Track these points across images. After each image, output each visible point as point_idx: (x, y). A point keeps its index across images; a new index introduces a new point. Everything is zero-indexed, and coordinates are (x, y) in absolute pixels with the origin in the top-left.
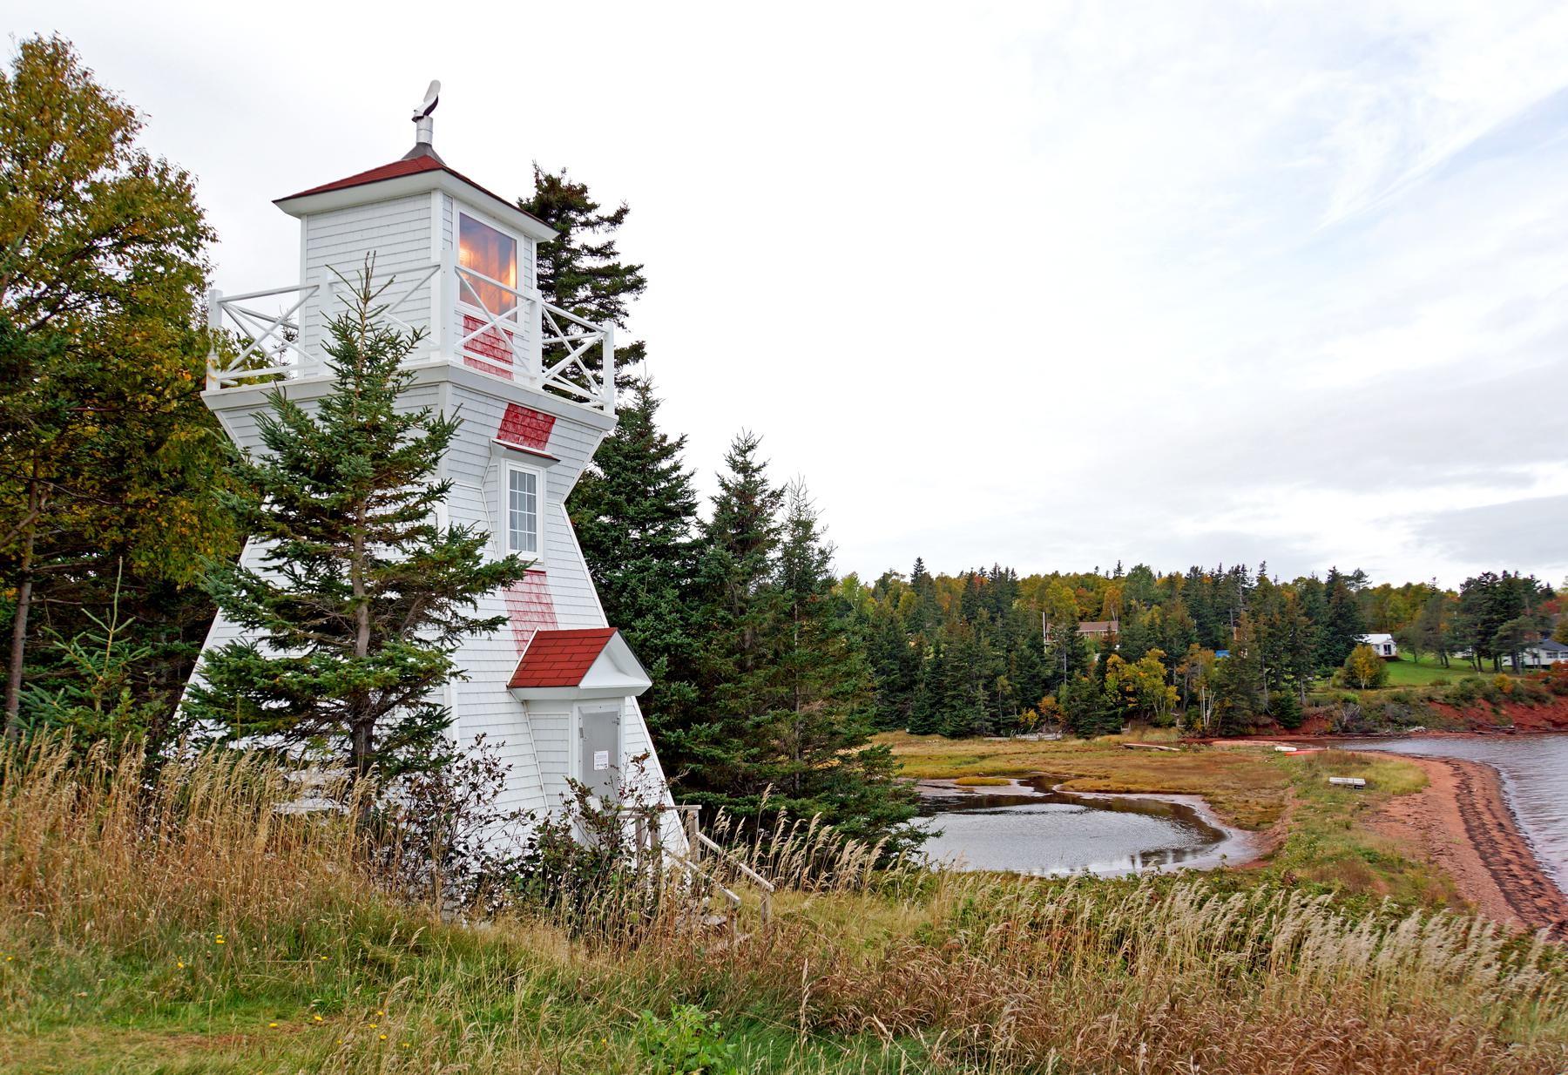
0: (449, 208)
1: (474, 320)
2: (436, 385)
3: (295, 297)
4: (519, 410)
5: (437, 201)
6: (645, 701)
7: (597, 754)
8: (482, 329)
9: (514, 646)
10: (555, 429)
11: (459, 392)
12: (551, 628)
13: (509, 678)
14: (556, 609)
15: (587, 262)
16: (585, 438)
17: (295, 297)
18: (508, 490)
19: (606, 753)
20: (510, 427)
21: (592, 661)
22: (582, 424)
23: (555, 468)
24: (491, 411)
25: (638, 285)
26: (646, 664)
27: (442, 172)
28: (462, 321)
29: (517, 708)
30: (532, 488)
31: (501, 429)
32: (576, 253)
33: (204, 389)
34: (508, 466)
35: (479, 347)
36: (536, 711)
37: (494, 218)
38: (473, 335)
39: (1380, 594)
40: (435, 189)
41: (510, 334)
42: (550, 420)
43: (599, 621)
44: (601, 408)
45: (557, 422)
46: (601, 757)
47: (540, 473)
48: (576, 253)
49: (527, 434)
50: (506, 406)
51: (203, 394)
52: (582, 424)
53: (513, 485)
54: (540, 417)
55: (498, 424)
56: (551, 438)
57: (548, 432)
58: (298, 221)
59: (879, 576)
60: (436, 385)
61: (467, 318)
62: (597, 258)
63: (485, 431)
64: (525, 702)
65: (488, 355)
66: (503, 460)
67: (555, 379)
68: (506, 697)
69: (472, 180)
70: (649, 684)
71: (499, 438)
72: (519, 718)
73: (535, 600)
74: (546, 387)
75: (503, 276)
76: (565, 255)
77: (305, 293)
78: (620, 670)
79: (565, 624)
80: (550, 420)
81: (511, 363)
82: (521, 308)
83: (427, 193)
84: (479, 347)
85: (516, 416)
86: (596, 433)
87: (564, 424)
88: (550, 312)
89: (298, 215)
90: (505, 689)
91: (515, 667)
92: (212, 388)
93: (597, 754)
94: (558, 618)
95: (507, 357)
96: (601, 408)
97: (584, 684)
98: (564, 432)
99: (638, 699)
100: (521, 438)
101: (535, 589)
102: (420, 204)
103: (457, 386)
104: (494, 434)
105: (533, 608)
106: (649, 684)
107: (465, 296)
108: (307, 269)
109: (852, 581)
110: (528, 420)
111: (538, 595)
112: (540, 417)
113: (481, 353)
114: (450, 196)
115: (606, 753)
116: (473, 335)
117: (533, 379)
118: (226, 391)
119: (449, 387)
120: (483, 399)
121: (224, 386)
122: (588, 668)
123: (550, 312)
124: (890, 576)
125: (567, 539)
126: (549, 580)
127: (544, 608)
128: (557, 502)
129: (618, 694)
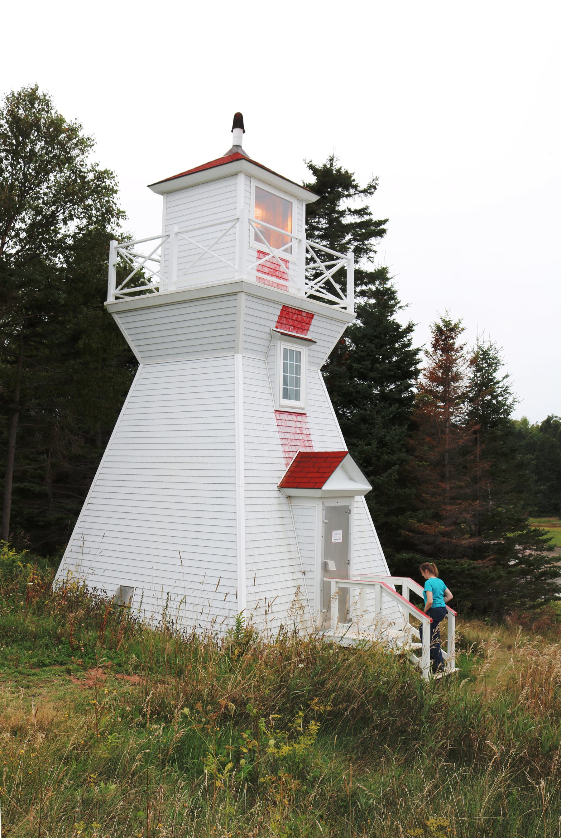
0: (248, 183)
1: (263, 253)
2: (236, 294)
3: (159, 241)
4: (290, 310)
5: (241, 180)
6: (368, 497)
7: (334, 532)
8: (267, 258)
9: (284, 461)
10: (313, 322)
11: (250, 298)
12: (308, 450)
13: (279, 481)
14: (312, 438)
15: (348, 220)
16: (334, 328)
17: (159, 241)
18: (282, 361)
19: (340, 532)
20: (284, 321)
21: (332, 472)
22: (332, 319)
23: (313, 347)
24: (271, 310)
25: (382, 233)
26: (368, 475)
27: (243, 161)
28: (256, 254)
29: (284, 501)
30: (298, 360)
31: (278, 322)
32: (342, 213)
33: (106, 300)
34: (282, 346)
35: (266, 270)
36: (295, 503)
37: (286, 192)
38: (261, 262)
39: (123, 277)
40: (241, 172)
41: (286, 261)
42: (311, 316)
43: (344, 447)
44: (345, 308)
45: (315, 317)
46: (337, 534)
47: (304, 351)
48: (342, 213)
49: (295, 325)
50: (281, 307)
51: (105, 303)
52: (332, 319)
53: (285, 358)
54: (304, 314)
55: (276, 318)
56: (311, 328)
57: (309, 324)
58: (161, 197)
59: (545, 418)
60: (236, 294)
61: (259, 252)
62: (356, 217)
63: (267, 323)
64: (289, 497)
65: (272, 275)
66: (279, 342)
67: (318, 291)
68: (276, 494)
69: (266, 166)
70: (371, 488)
71: (277, 327)
72: (285, 507)
73: (298, 432)
74: (311, 297)
75: (284, 227)
76: (335, 215)
77: (164, 239)
78: (351, 479)
79: (318, 448)
80: (311, 316)
81: (287, 280)
82: (294, 244)
83: (235, 175)
84: (266, 270)
85: (288, 314)
86: (342, 325)
87: (319, 318)
88: (311, 247)
89: (162, 193)
90: (277, 489)
91: (283, 474)
92: (111, 299)
93: (334, 532)
94: (314, 444)
95: (285, 276)
96: (345, 308)
97: (326, 487)
98: (320, 324)
99: (365, 497)
100: (292, 328)
101: (298, 425)
102: (231, 182)
103: (248, 294)
104: (273, 325)
105: (297, 437)
106: (371, 488)
107: (257, 239)
108: (166, 225)
109: (525, 422)
110: (295, 316)
111: (301, 428)
112: (304, 314)
113: (268, 274)
114: (250, 176)
115: (340, 532)
116: (261, 262)
117: (299, 290)
118: (118, 301)
119: (243, 296)
120: (266, 303)
121: (117, 298)
122: (328, 477)
123: (311, 247)
124: (552, 418)
125: (322, 393)
126: (308, 419)
127: (304, 437)
128: (316, 369)
129: (350, 495)
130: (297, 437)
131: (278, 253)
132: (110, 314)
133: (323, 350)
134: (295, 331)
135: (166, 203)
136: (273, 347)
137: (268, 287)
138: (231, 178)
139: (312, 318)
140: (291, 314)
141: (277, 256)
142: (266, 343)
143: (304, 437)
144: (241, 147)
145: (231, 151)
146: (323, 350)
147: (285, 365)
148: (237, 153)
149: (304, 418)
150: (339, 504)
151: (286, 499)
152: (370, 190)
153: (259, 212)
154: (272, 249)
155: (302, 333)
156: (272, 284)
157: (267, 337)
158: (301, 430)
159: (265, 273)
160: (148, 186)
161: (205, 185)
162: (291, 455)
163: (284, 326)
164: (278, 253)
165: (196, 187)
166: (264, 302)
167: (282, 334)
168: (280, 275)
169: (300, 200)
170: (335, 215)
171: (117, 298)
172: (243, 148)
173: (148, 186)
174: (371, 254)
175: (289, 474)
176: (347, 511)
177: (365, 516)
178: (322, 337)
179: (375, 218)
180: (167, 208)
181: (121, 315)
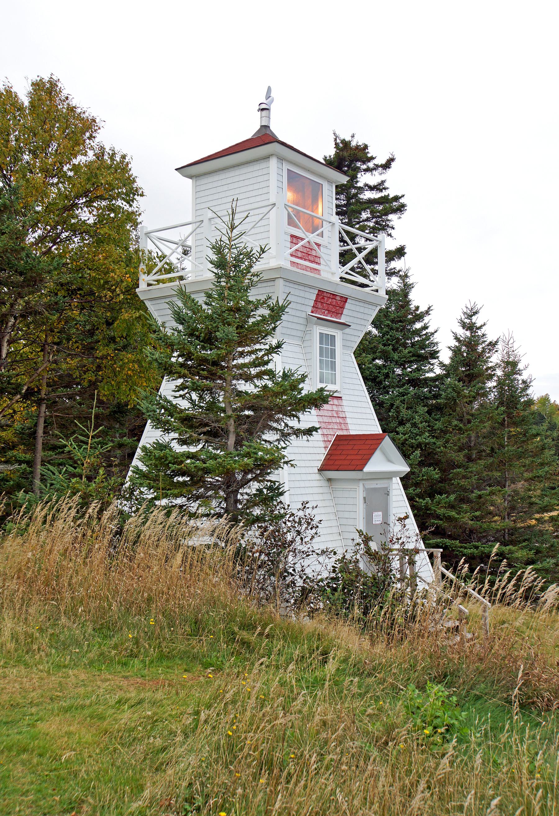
0: (280, 166)
2: (273, 280)
4: (325, 294)
5: (273, 163)
7: (375, 514)
8: (302, 243)
10: (347, 306)
11: (287, 284)
12: (345, 433)
13: (319, 464)
14: (348, 421)
15: (368, 195)
16: (366, 311)
18: (318, 345)
19: (380, 513)
20: (319, 305)
21: (372, 454)
23: (347, 330)
24: (307, 295)
25: (401, 209)
26: (406, 456)
28: (289, 239)
29: (325, 484)
30: (333, 343)
32: (361, 190)
34: (318, 330)
35: (300, 254)
38: (296, 247)
41: (318, 245)
42: (344, 300)
43: (375, 428)
44: (377, 291)
45: (348, 301)
46: (377, 516)
47: (338, 334)
48: (361, 190)
49: (330, 309)
50: (316, 292)
51: (137, 290)
52: (365, 302)
53: (321, 343)
54: (338, 298)
55: (312, 303)
56: (345, 312)
57: (343, 308)
60: (273, 280)
61: (292, 236)
63: (303, 308)
64: (329, 480)
65: (305, 260)
66: (315, 326)
67: (347, 273)
68: (317, 477)
70: (408, 469)
71: (312, 312)
72: (326, 490)
73: (335, 415)
76: (353, 191)
78: (389, 461)
80: (344, 300)
82: (326, 227)
84: (300, 254)
86: (374, 308)
87: (353, 302)
89: (191, 177)
90: (317, 471)
91: (323, 457)
92: (143, 286)
93: (375, 514)
94: (350, 427)
95: (317, 260)
98: (353, 308)
100: (326, 312)
102: (263, 165)
103: (286, 280)
104: (309, 310)
105: (334, 420)
106: (408, 469)
107: (291, 222)
110: (330, 300)
111: (337, 412)
112: (338, 298)
113: (301, 258)
114: (281, 159)
115: (380, 513)
116: (296, 247)
117: (333, 274)
118: (150, 288)
119: (281, 281)
120: (302, 288)
121: (149, 285)
127: (341, 420)
128: (349, 352)
129: (388, 476)
130: (334, 420)
131: (313, 238)
132: (142, 302)
133: (356, 333)
134: (329, 315)
135: (195, 186)
136: (309, 332)
137: (305, 272)
138: (262, 161)
139: (346, 302)
140: (326, 299)
141: (312, 241)
142: (302, 328)
143: (341, 420)
144: (269, 127)
145: (259, 131)
146: (356, 333)
147: (321, 348)
148: (266, 134)
149: (340, 401)
150: (378, 486)
151: (326, 482)
152: (387, 166)
153: (290, 195)
154: (307, 234)
155: (336, 317)
156: (306, 268)
157: (303, 321)
158: (337, 414)
159: (298, 257)
160: (176, 170)
161: (236, 168)
162: (330, 438)
163: (319, 310)
164: (313, 238)
165: (227, 171)
166: (301, 288)
167: (319, 318)
168: (312, 259)
169: (330, 182)
170: (353, 191)
171: (149, 285)
172: (271, 128)
173: (176, 170)
174: (390, 231)
175: (328, 457)
176: (387, 493)
177: (401, 498)
178: (355, 321)
179: (392, 193)
180: (196, 192)
181: (154, 302)
